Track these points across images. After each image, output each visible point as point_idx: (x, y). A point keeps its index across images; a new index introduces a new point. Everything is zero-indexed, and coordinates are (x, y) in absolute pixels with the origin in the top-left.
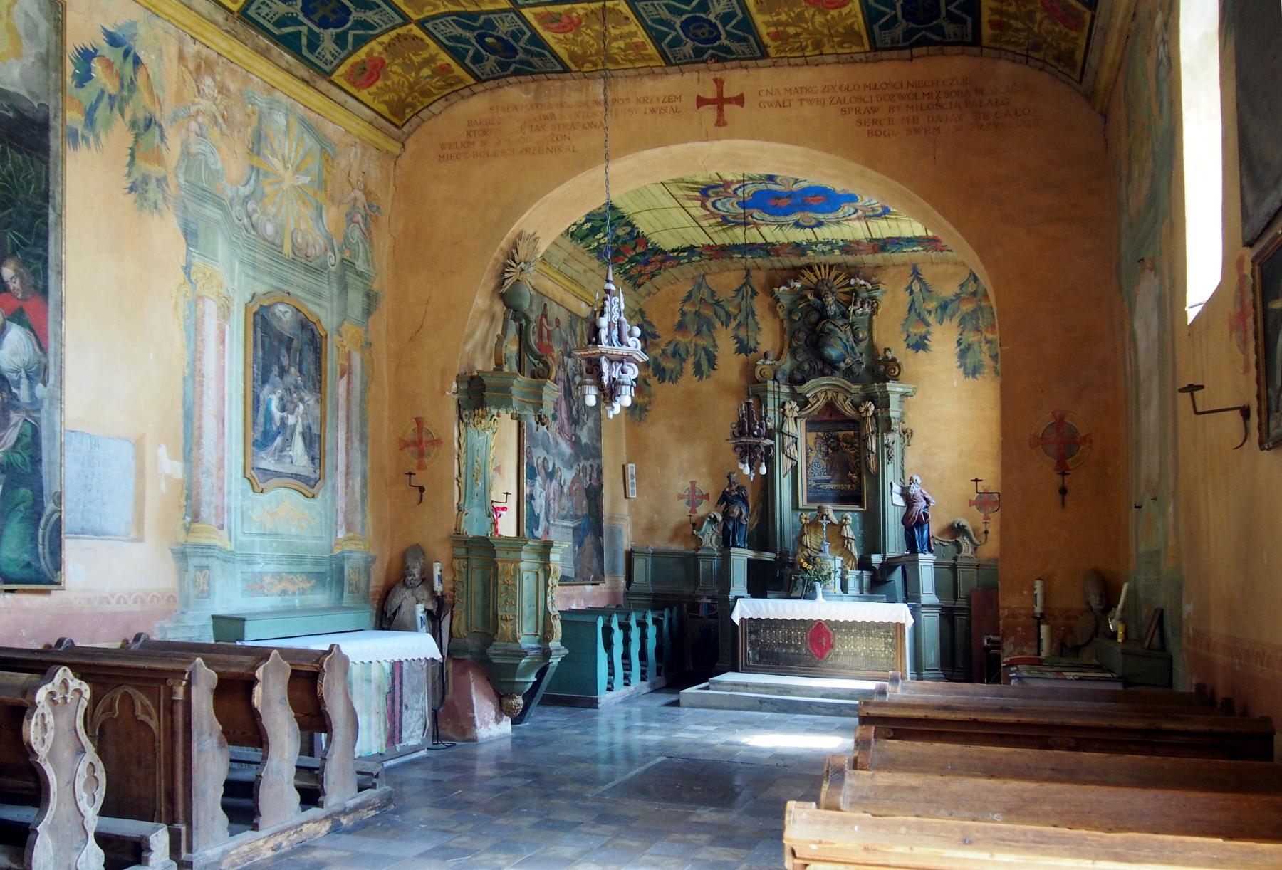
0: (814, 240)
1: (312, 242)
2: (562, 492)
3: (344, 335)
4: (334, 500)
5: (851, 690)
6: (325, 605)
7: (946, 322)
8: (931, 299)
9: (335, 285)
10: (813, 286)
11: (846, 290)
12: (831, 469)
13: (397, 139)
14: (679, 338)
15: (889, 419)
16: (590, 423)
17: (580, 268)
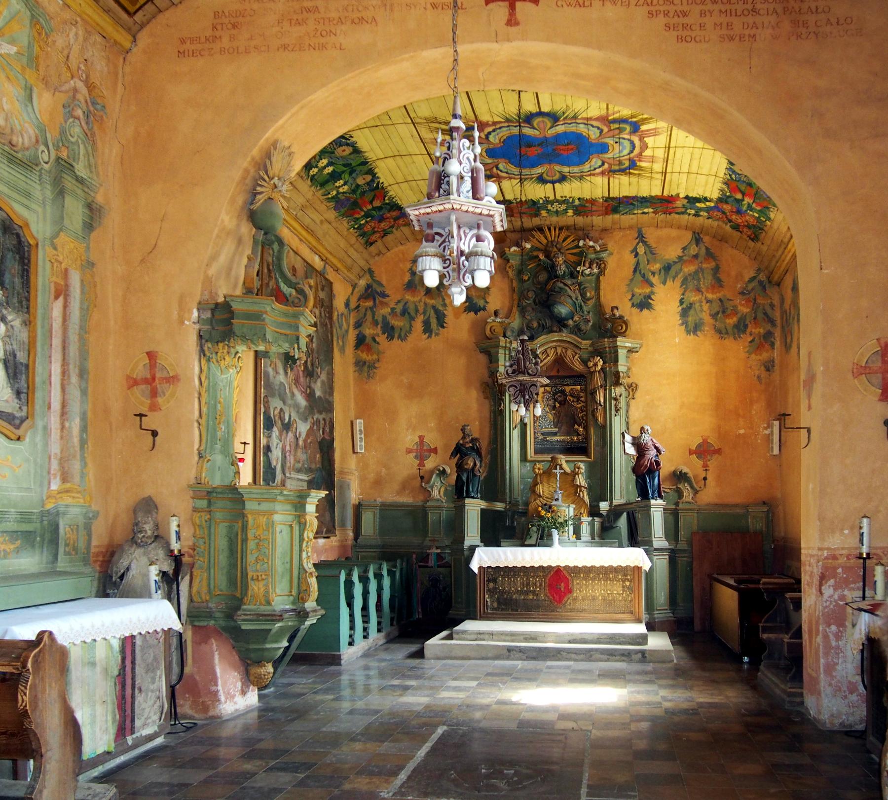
0: (552, 198)
1: (18, 127)
2: (297, 445)
3: (60, 249)
4: (46, 445)
5: (599, 634)
6: (34, 569)
7: (669, 283)
8: (655, 261)
9: (49, 187)
10: (542, 247)
11: (574, 251)
12: (558, 422)
13: (129, 30)
14: (408, 297)
15: (618, 372)
16: (323, 377)
17: (317, 218)
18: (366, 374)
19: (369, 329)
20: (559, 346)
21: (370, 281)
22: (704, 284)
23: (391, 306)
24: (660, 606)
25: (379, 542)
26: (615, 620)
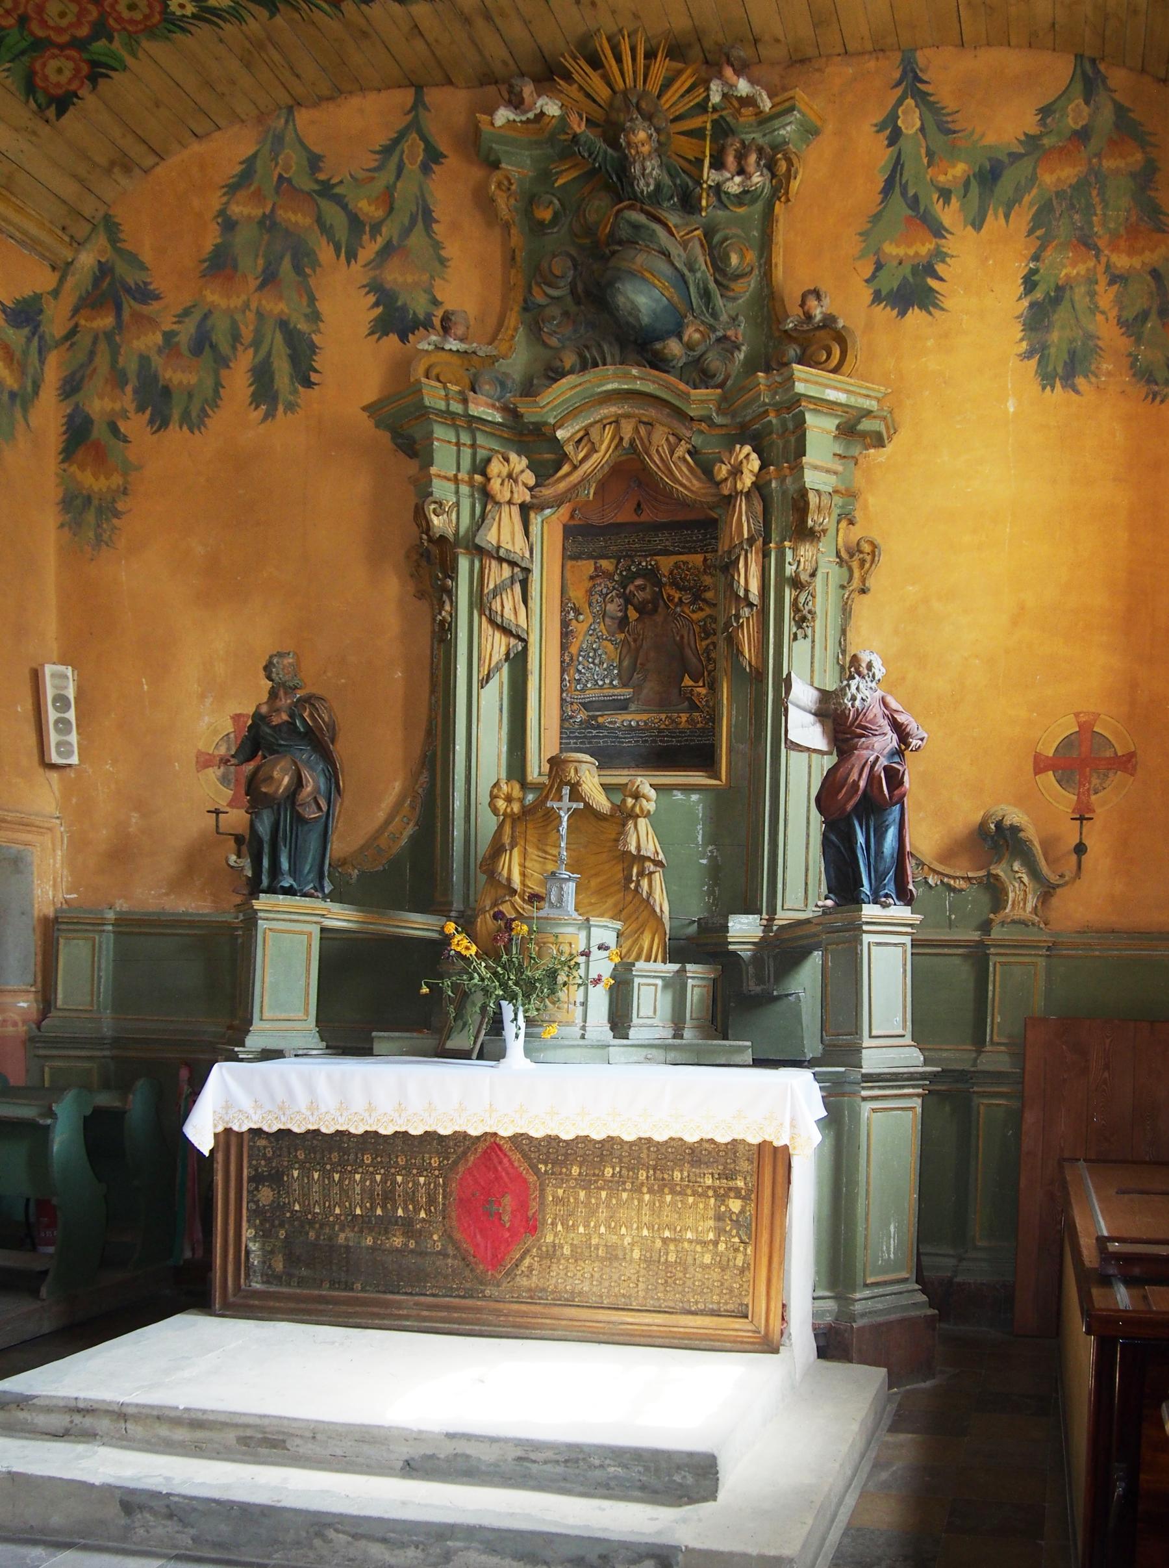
5: (455, 1483)
7: (994, 222)
12: (633, 668)
14: (213, 297)
15: (803, 493)
18: (91, 534)
19: (101, 398)
20: (627, 416)
21: (109, 255)
22: (1104, 224)
23: (167, 327)
24: (884, 1270)
25: (107, 1029)
26: (688, 1337)
